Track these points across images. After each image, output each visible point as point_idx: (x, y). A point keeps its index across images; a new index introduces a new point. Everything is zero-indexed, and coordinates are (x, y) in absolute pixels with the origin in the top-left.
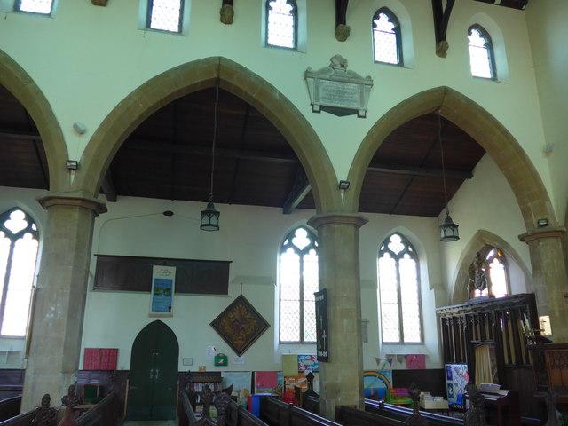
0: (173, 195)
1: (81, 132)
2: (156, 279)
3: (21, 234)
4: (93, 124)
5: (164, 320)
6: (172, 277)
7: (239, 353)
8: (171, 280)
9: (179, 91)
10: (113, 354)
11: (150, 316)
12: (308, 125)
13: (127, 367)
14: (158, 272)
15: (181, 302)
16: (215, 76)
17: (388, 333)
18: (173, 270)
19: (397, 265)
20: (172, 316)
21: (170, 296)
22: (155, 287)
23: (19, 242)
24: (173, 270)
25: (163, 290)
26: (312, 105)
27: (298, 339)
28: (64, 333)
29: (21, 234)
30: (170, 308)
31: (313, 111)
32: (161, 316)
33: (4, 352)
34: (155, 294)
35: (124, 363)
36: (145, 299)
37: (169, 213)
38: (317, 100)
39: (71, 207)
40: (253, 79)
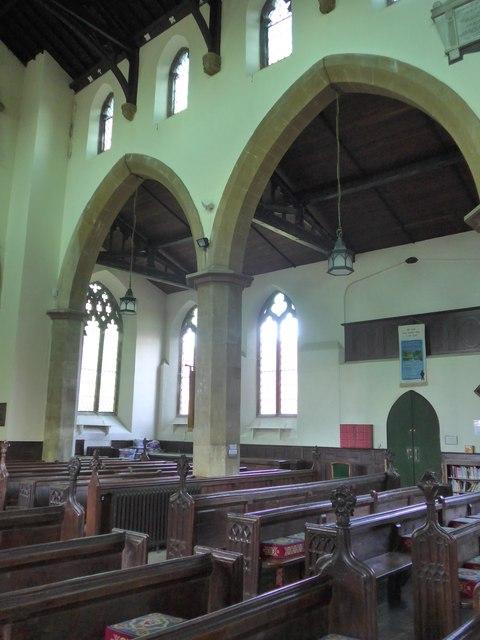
0: (412, 237)
1: (210, 208)
2: (404, 342)
3: (283, 315)
4: (216, 196)
5: (419, 390)
6: (422, 336)
7: (370, 428)
8: (420, 341)
9: (295, 122)
10: (368, 430)
11: (402, 386)
12: (444, 88)
13: (384, 446)
14: (406, 333)
15: (435, 365)
16: (326, 83)
17: (268, 407)
18: (421, 328)
19: (279, 329)
20: (426, 384)
21: (422, 360)
22: (403, 352)
23: (284, 322)
24: (421, 328)
25: (411, 354)
26: (447, 54)
27: (274, 412)
28: (210, 407)
29: (283, 315)
30: (422, 374)
31: (451, 62)
32: (413, 385)
33: (277, 429)
34: (404, 359)
35: (381, 441)
36: (392, 368)
37: (412, 260)
38: (452, 42)
39: (206, 283)
40: (363, 64)
